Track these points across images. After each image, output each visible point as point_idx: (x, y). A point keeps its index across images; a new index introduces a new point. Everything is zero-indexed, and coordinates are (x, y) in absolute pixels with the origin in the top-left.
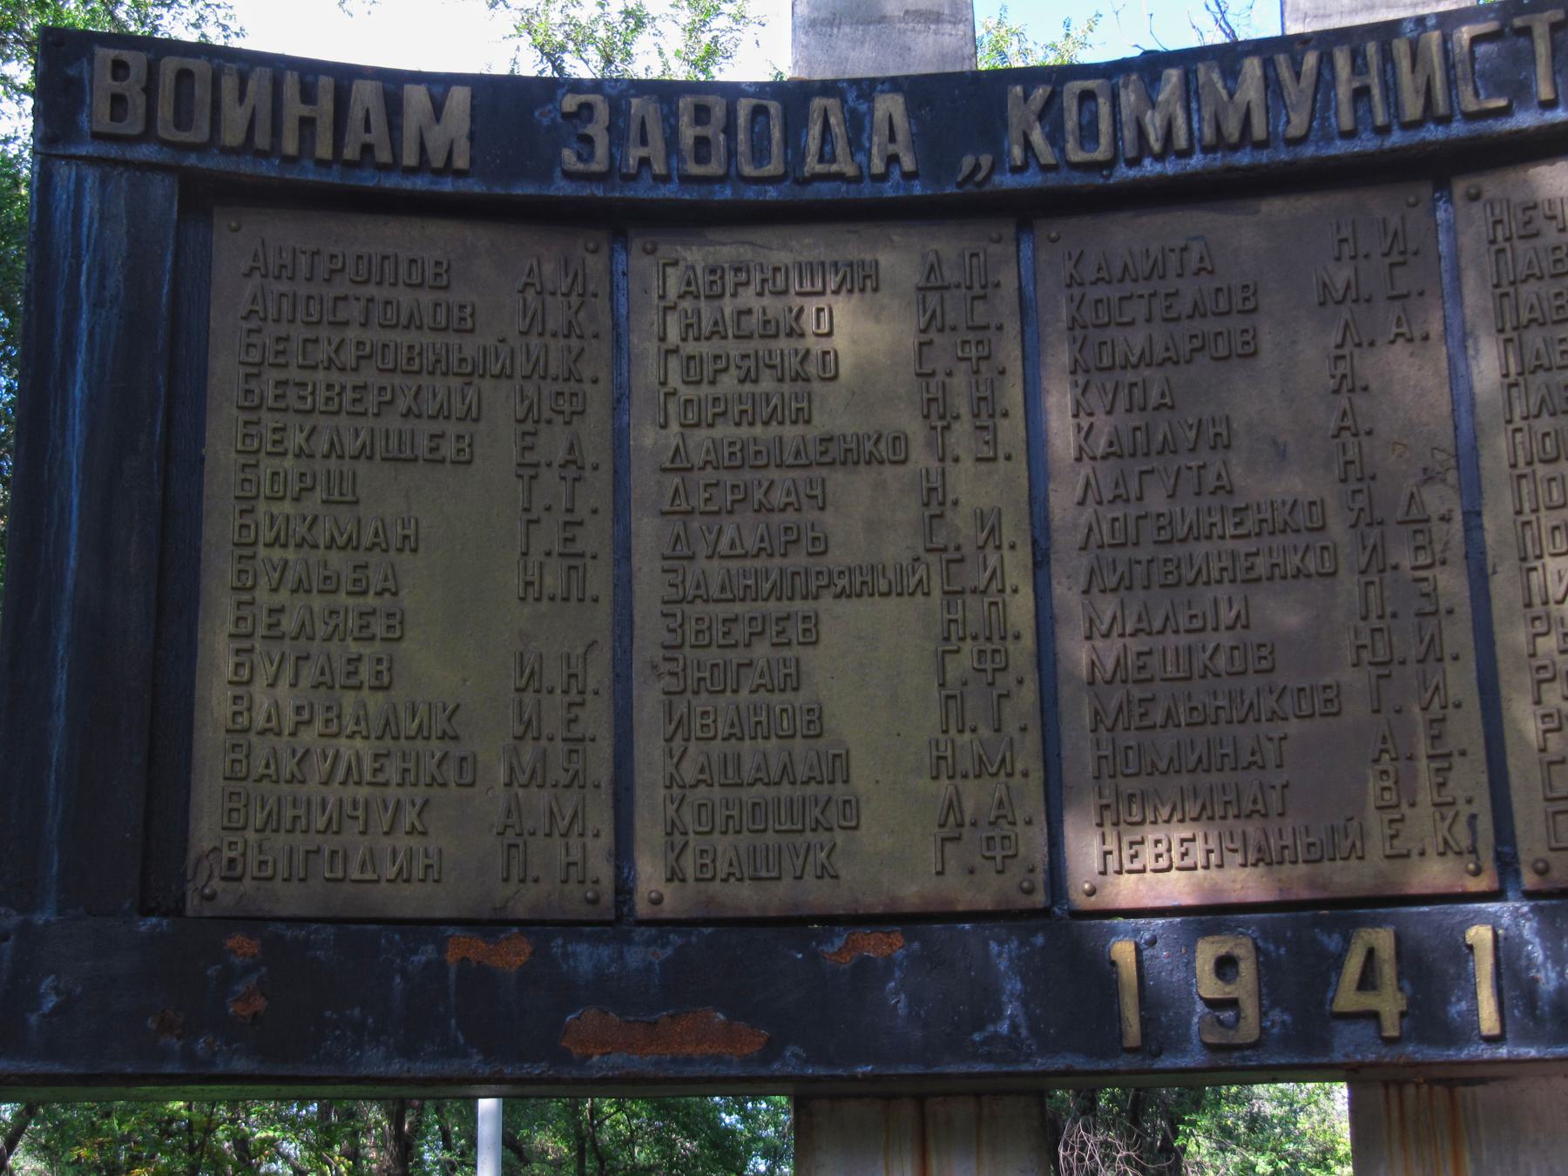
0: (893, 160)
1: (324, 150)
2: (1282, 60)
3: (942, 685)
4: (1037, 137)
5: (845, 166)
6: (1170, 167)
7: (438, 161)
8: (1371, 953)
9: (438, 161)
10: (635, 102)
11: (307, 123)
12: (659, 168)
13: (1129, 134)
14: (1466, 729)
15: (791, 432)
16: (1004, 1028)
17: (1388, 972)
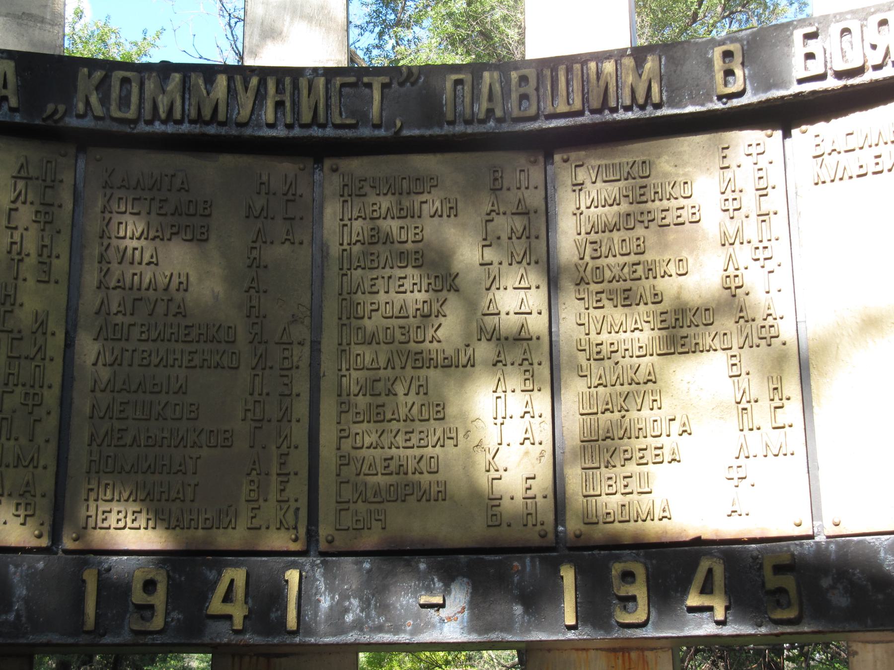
4: (94, 99)
6: (170, 129)
14: (299, 461)
16: (12, 617)
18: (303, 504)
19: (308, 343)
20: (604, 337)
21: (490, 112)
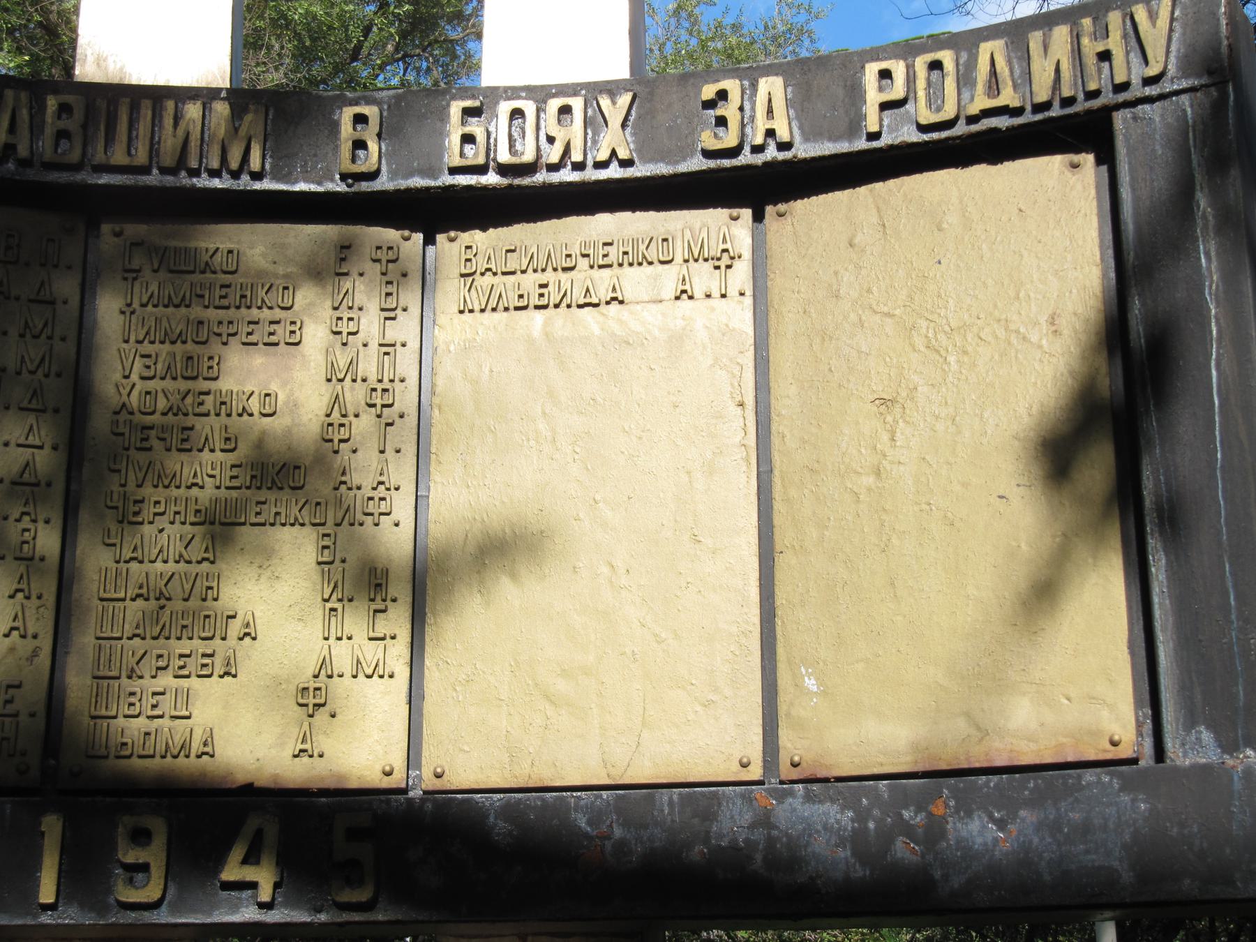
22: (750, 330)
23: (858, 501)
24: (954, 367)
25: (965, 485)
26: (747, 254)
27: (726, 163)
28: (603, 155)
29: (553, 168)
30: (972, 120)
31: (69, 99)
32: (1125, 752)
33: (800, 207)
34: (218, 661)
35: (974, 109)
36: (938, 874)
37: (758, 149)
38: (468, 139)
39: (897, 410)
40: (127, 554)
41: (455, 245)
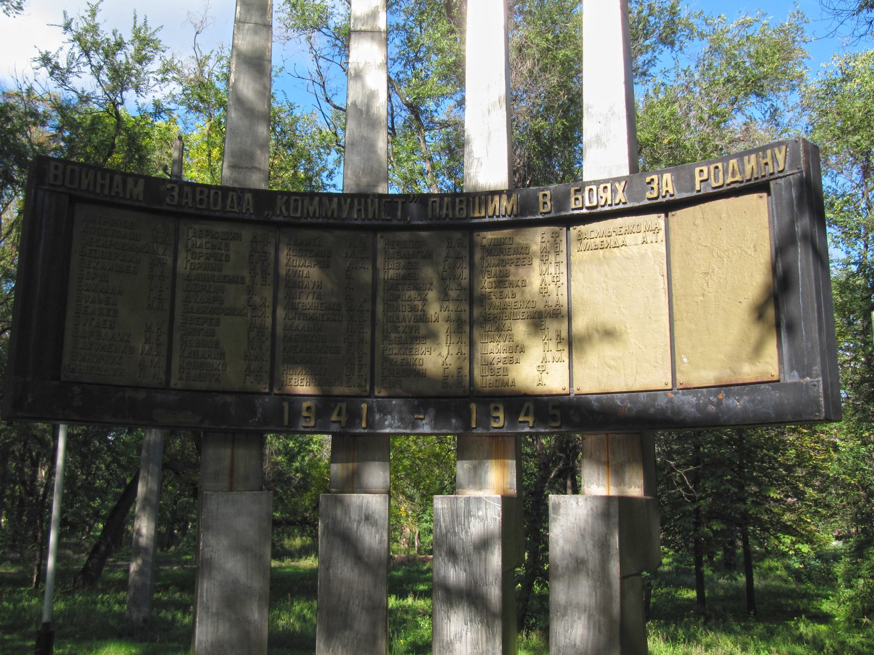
0: (248, 209)
1: (106, 192)
2: (342, 199)
3: (249, 338)
4: (283, 209)
5: (236, 210)
6: (314, 221)
7: (135, 198)
8: (341, 408)
9: (135, 198)
10: (185, 187)
11: (103, 185)
12: (190, 205)
13: (305, 211)
14: (367, 359)
15: (217, 273)
16: (257, 420)
17: (344, 412)
18: (368, 377)
19: (370, 311)
20: (492, 311)
21: (447, 215)
22: (665, 252)
23: (698, 304)
24: (726, 262)
25: (729, 299)
26: (663, 228)
27: (654, 201)
28: (617, 202)
29: (602, 206)
30: (728, 185)
31: (462, 198)
32: (775, 378)
33: (679, 212)
34: (515, 359)
35: (728, 182)
36: (720, 415)
37: (664, 197)
38: (577, 199)
39: (709, 276)
40: (487, 330)
41: (576, 231)
